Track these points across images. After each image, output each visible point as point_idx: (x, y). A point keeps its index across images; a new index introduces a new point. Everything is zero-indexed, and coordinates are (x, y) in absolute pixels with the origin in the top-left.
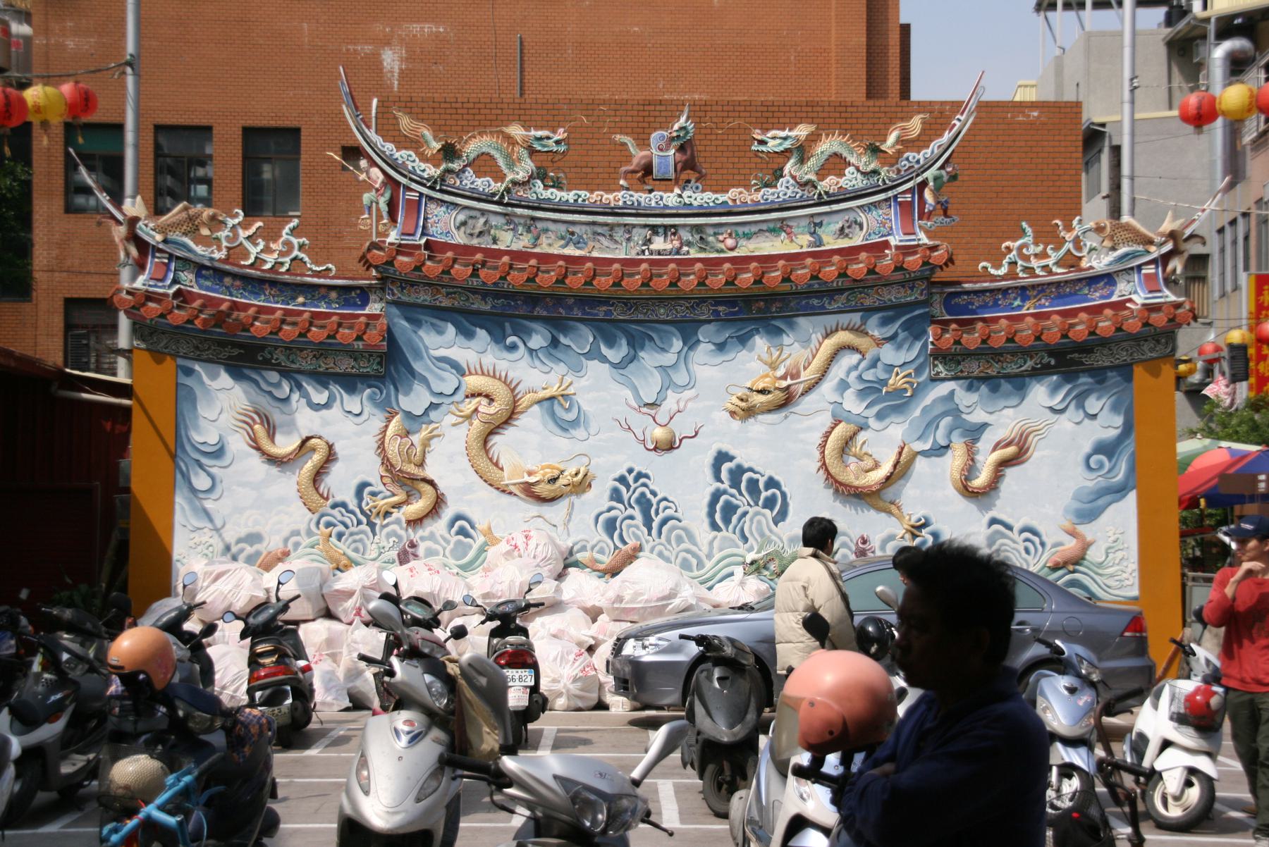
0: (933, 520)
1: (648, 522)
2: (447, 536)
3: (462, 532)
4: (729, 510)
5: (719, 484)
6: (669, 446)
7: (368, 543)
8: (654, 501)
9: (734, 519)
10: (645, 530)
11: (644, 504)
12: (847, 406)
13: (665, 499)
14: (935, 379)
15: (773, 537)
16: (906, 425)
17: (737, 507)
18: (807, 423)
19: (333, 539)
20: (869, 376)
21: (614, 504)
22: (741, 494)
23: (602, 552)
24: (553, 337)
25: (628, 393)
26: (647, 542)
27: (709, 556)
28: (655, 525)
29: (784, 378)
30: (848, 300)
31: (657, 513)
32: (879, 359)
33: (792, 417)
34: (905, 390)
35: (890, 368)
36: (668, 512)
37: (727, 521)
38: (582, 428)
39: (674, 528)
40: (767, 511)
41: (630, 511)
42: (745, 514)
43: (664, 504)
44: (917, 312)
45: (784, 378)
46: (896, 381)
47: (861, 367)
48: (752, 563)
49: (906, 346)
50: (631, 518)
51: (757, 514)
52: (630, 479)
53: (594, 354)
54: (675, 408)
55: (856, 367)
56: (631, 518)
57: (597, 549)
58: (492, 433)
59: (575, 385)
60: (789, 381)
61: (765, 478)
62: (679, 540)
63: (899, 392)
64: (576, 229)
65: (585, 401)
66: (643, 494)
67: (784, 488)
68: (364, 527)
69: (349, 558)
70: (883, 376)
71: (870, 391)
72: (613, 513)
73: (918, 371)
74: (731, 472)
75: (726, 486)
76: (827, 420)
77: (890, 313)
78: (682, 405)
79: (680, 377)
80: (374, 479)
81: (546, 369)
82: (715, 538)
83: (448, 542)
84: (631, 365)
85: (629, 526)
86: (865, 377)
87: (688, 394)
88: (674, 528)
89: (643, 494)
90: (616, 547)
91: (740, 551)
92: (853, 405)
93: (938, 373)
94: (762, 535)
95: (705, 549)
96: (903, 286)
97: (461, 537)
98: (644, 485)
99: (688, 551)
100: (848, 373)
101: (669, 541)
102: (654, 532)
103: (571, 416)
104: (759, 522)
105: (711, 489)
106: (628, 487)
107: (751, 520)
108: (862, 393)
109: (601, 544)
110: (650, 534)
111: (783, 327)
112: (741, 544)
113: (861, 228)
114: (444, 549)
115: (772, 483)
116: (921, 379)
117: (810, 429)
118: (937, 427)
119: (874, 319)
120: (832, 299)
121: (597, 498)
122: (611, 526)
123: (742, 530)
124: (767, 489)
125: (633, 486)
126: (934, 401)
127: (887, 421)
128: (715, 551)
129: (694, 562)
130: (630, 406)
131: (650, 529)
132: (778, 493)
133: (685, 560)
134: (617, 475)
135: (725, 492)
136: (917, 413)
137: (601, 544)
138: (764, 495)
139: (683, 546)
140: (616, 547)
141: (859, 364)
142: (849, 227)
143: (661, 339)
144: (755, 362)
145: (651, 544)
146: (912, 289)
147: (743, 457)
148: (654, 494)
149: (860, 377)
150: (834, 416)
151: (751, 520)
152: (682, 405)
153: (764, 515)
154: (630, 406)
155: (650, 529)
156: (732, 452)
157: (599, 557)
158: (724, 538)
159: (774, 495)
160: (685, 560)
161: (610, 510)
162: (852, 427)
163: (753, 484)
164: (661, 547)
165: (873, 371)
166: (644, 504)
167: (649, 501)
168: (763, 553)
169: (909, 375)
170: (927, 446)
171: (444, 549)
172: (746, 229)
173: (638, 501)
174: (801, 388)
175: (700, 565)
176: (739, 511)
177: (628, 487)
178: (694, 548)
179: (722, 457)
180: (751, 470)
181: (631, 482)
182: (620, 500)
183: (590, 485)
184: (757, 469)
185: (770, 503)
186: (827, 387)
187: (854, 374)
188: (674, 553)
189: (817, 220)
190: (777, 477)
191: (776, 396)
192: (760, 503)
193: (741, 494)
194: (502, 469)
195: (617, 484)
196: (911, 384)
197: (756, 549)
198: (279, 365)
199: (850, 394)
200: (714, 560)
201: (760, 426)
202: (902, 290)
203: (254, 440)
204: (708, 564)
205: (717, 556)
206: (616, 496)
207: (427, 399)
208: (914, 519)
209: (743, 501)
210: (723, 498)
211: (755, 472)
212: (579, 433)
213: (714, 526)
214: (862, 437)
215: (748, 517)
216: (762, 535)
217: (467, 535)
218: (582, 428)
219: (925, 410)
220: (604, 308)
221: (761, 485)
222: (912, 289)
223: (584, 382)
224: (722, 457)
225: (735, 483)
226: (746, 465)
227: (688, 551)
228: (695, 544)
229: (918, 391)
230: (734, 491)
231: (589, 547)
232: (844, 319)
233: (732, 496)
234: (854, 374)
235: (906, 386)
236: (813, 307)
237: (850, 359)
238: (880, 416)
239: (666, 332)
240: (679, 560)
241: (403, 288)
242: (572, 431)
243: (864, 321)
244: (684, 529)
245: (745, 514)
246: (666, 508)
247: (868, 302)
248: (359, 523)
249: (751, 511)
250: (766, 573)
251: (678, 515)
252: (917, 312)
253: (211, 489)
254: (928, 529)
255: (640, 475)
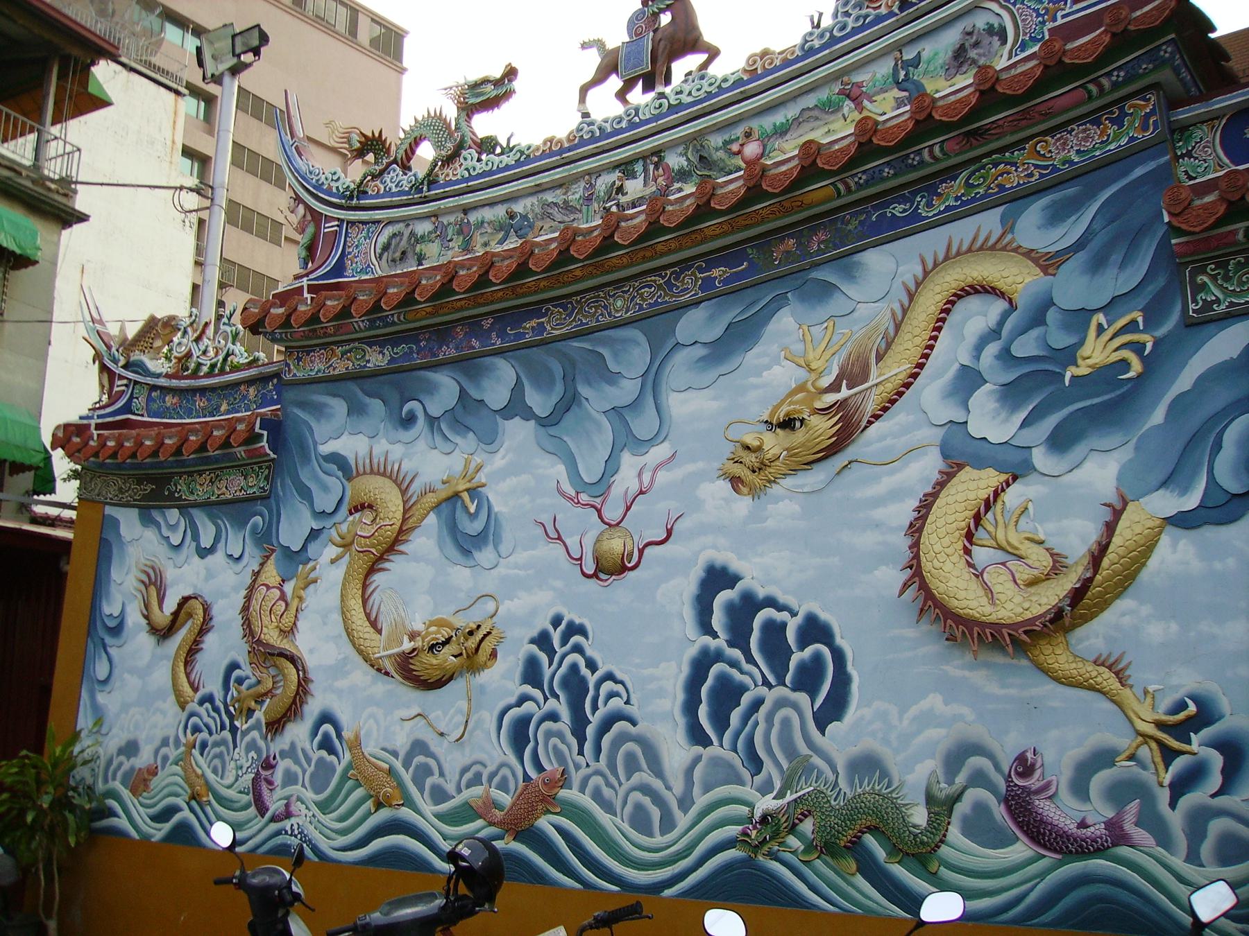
0: (1224, 704)
1: (579, 729)
2: (308, 747)
3: (326, 745)
4: (728, 694)
5: (707, 639)
6: (611, 568)
7: (227, 758)
8: (592, 680)
9: (735, 717)
10: (574, 742)
11: (575, 686)
12: (975, 430)
13: (610, 677)
14: (1205, 322)
15: (817, 760)
16: (1126, 454)
17: (743, 689)
18: (887, 483)
19: (196, 752)
20: (1026, 346)
21: (528, 689)
22: (750, 659)
23: (503, 786)
24: (462, 390)
25: (559, 470)
26: (577, 767)
27: (685, 802)
28: (590, 731)
29: (834, 387)
30: (968, 185)
31: (595, 708)
32: (1049, 303)
33: (856, 472)
34: (1124, 364)
35: (1079, 319)
36: (616, 703)
37: (721, 723)
38: (491, 547)
39: (623, 738)
40: (802, 698)
41: (552, 702)
42: (757, 704)
43: (608, 686)
44: (1139, 172)
45: (834, 387)
46: (1097, 351)
47: (1005, 332)
48: (764, 819)
49: (1117, 257)
50: (553, 717)
51: (781, 703)
52: (556, 637)
53: (516, 407)
54: (634, 487)
55: (995, 333)
56: (553, 717)
57: (496, 780)
58: (372, 570)
59: (486, 470)
60: (845, 392)
61: (799, 619)
62: (632, 766)
63: (1109, 374)
64: (518, 208)
65: (500, 498)
66: (574, 668)
67: (839, 641)
68: (226, 734)
69: (207, 783)
70: (1060, 340)
71: (1034, 383)
72: (529, 706)
73: (1153, 314)
74: (730, 608)
75: (720, 643)
76: (929, 465)
77: (1070, 191)
78: (646, 478)
79: (643, 425)
80: (243, 659)
81: (448, 447)
82: (698, 759)
83: (309, 760)
84: (569, 416)
85: (549, 734)
86: (1017, 351)
87: (659, 452)
88: (623, 738)
89: (574, 668)
90: (527, 778)
91: (747, 792)
92: (990, 422)
93: (1208, 305)
94: (791, 752)
95: (678, 787)
96: (1097, 122)
97: (324, 753)
98: (578, 649)
99: (645, 789)
100: (979, 348)
101: (612, 766)
102: (588, 746)
103: (475, 527)
104: (786, 722)
105: (692, 651)
106: (551, 653)
107: (770, 719)
108: (1011, 394)
109: (505, 771)
110: (581, 753)
111: (832, 279)
112: (746, 775)
113: (1004, 40)
114: (304, 772)
115: (815, 630)
116: (1161, 332)
117: (896, 495)
118: (1218, 446)
119: (1033, 213)
120: (932, 191)
121: (501, 679)
122: (520, 735)
123: (750, 743)
124: (803, 644)
125: (560, 651)
126: (1201, 379)
127: (1079, 450)
128: (696, 790)
129: (655, 813)
130: (562, 494)
131: (581, 740)
132: (826, 651)
133: (639, 807)
134: (534, 633)
135: (718, 656)
136: (1158, 416)
137: (505, 771)
138: (796, 658)
139: (637, 778)
140: (527, 778)
141: (1001, 323)
142: (976, 45)
143: (616, 355)
144: (791, 353)
145: (584, 771)
146: (1118, 122)
147: (758, 572)
148: (592, 666)
149: (1006, 356)
150: (945, 455)
151: (770, 719)
152: (646, 478)
153: (795, 706)
154: (562, 494)
155: (581, 740)
156: (736, 564)
157: (497, 794)
158: (716, 762)
159: (817, 659)
160: (639, 807)
161: (519, 703)
162: (992, 478)
163: (774, 631)
164: (597, 780)
165: (1035, 333)
166: (575, 686)
167: (583, 682)
168: (789, 797)
169: (1131, 327)
170: (1191, 501)
171: (304, 772)
172: (779, 118)
173: (565, 683)
174: (870, 407)
175: (668, 823)
176: (746, 699)
177: (551, 653)
178: (657, 784)
179: (717, 578)
180: (771, 602)
181: (556, 643)
182: (537, 684)
183: (494, 655)
184: (782, 598)
185: (808, 679)
186: (930, 394)
187: (992, 349)
188: (622, 791)
189: (909, 55)
190: (824, 616)
191: (822, 428)
192: (788, 679)
193: (750, 659)
194: (379, 632)
195: (534, 648)
196: (1138, 348)
197: (778, 784)
198: (180, 499)
199: (983, 399)
200: (693, 811)
201: (787, 501)
202: (1094, 130)
203: (147, 606)
204: (683, 820)
205: (701, 801)
206: (532, 673)
207: (310, 523)
208: (1166, 702)
209: (753, 674)
210: (716, 669)
211: (780, 608)
212: (485, 556)
213: (697, 736)
214: (1013, 497)
215: (763, 710)
216: (791, 752)
217: (332, 751)
218: (491, 547)
219: (1179, 406)
220: (533, 323)
221: (791, 636)
222: (1118, 122)
223: (499, 461)
224: (717, 578)
225: (739, 638)
226: (761, 593)
227: (645, 789)
228: (659, 773)
229: (1158, 362)
230: (736, 653)
231: (484, 778)
232: (962, 231)
233: (734, 664)
234: (992, 349)
235: (1127, 354)
236: (895, 221)
237: (977, 317)
238: (1060, 441)
239: (625, 341)
240: (629, 808)
241: (299, 359)
242: (476, 554)
243: (1008, 225)
244: (641, 740)
245: (757, 704)
246: (611, 695)
247: (1014, 179)
248: (223, 727)
249: (771, 696)
250: (793, 841)
251: (632, 710)
252: (1139, 172)
253: (105, 682)
254: (1206, 732)
255: (575, 629)
